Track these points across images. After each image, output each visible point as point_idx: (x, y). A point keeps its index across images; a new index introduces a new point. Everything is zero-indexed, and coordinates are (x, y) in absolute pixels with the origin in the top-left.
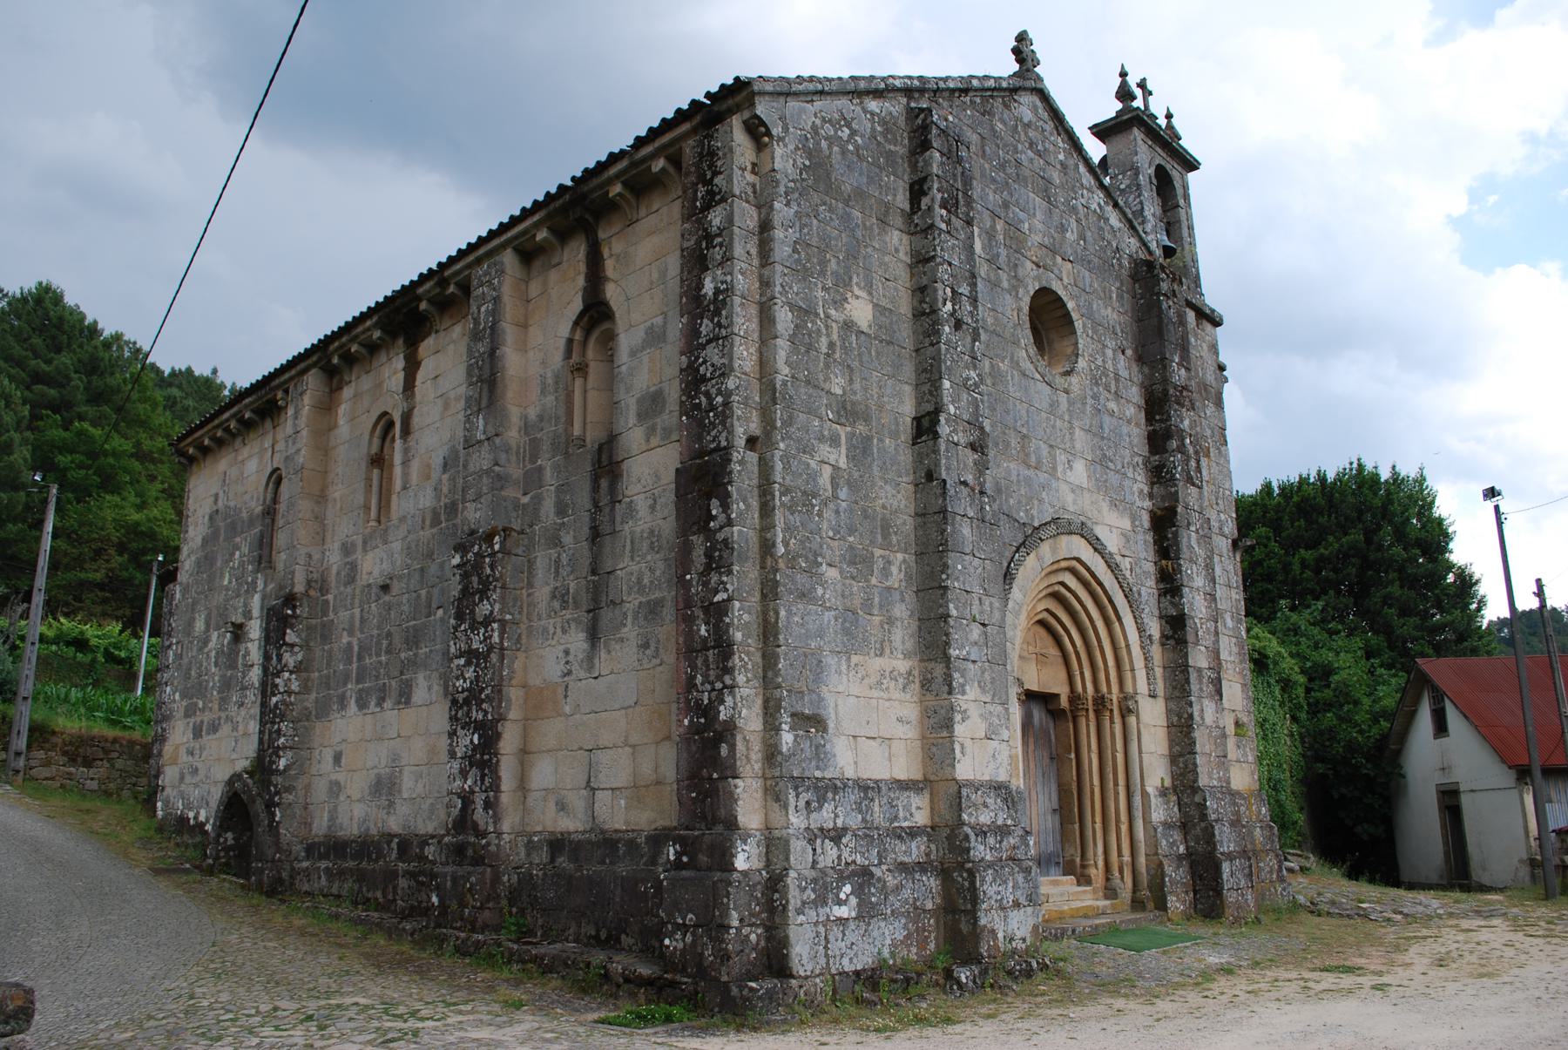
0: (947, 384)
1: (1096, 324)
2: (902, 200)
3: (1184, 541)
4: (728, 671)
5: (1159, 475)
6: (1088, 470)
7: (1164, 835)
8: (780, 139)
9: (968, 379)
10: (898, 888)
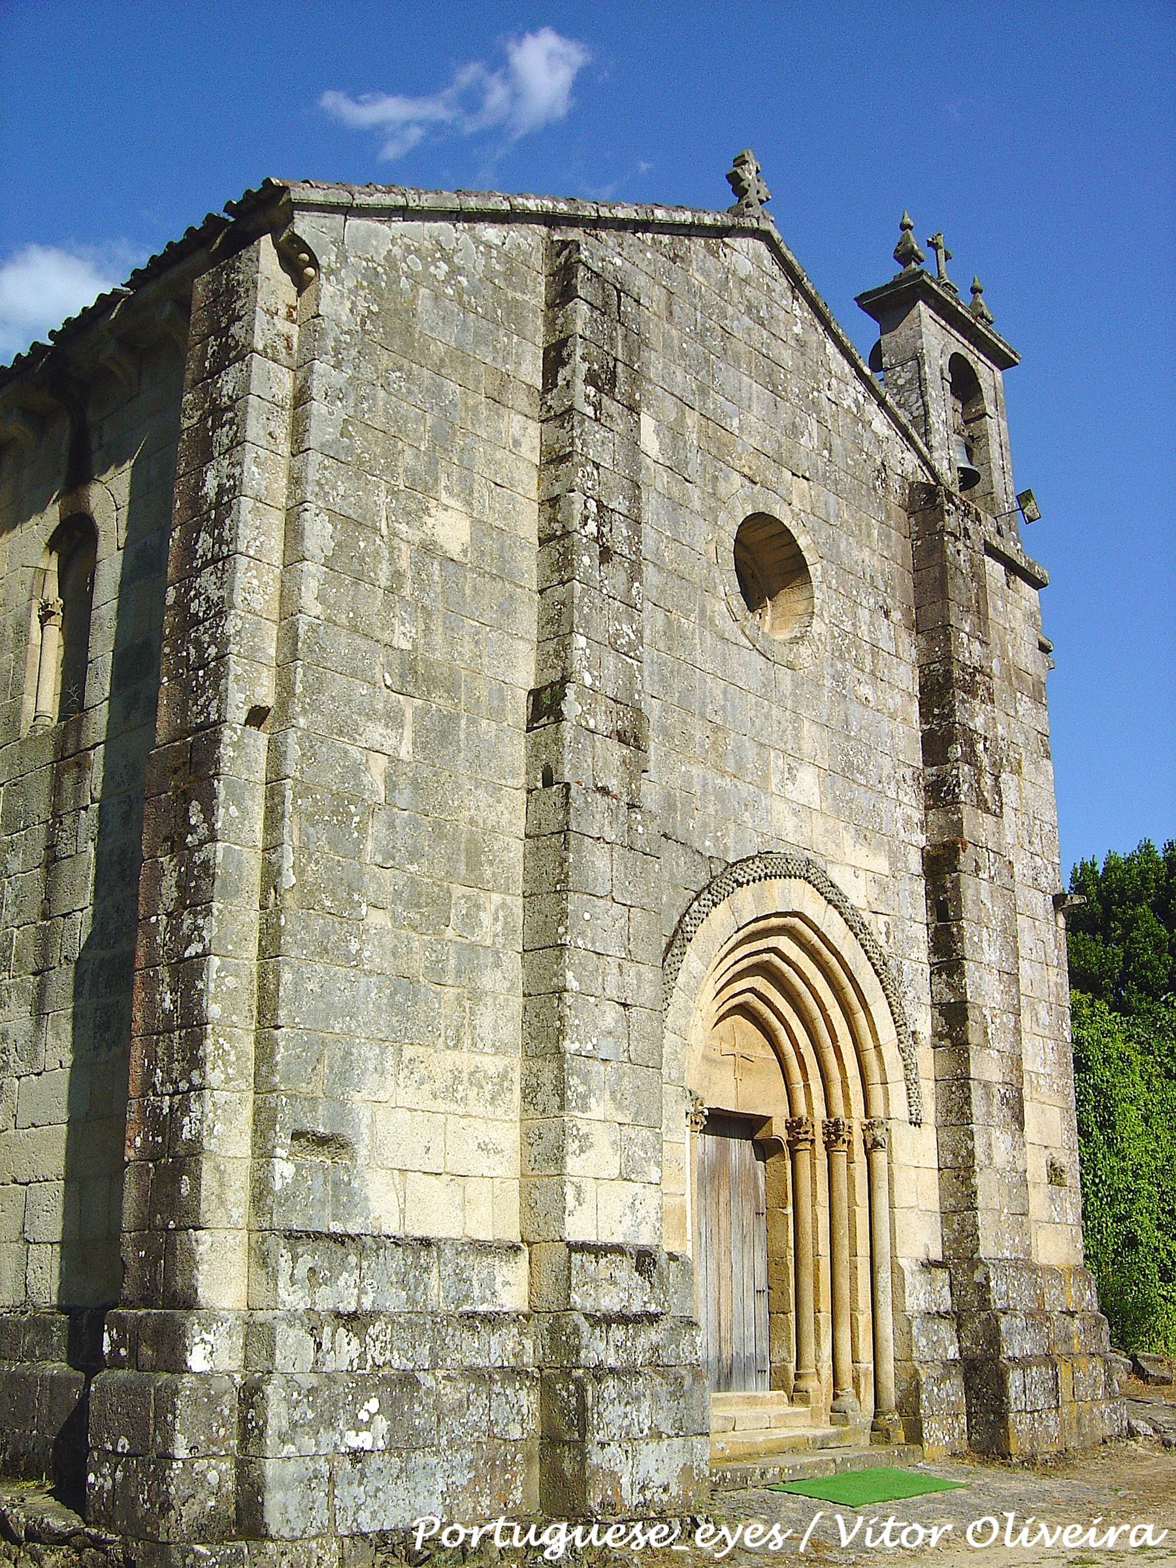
0: (581, 641)
1: (845, 571)
2: (532, 371)
3: (968, 895)
4: (197, 1063)
5: (939, 794)
6: (821, 783)
7: (924, 1332)
8: (332, 272)
9: (618, 636)
10: (462, 1406)
